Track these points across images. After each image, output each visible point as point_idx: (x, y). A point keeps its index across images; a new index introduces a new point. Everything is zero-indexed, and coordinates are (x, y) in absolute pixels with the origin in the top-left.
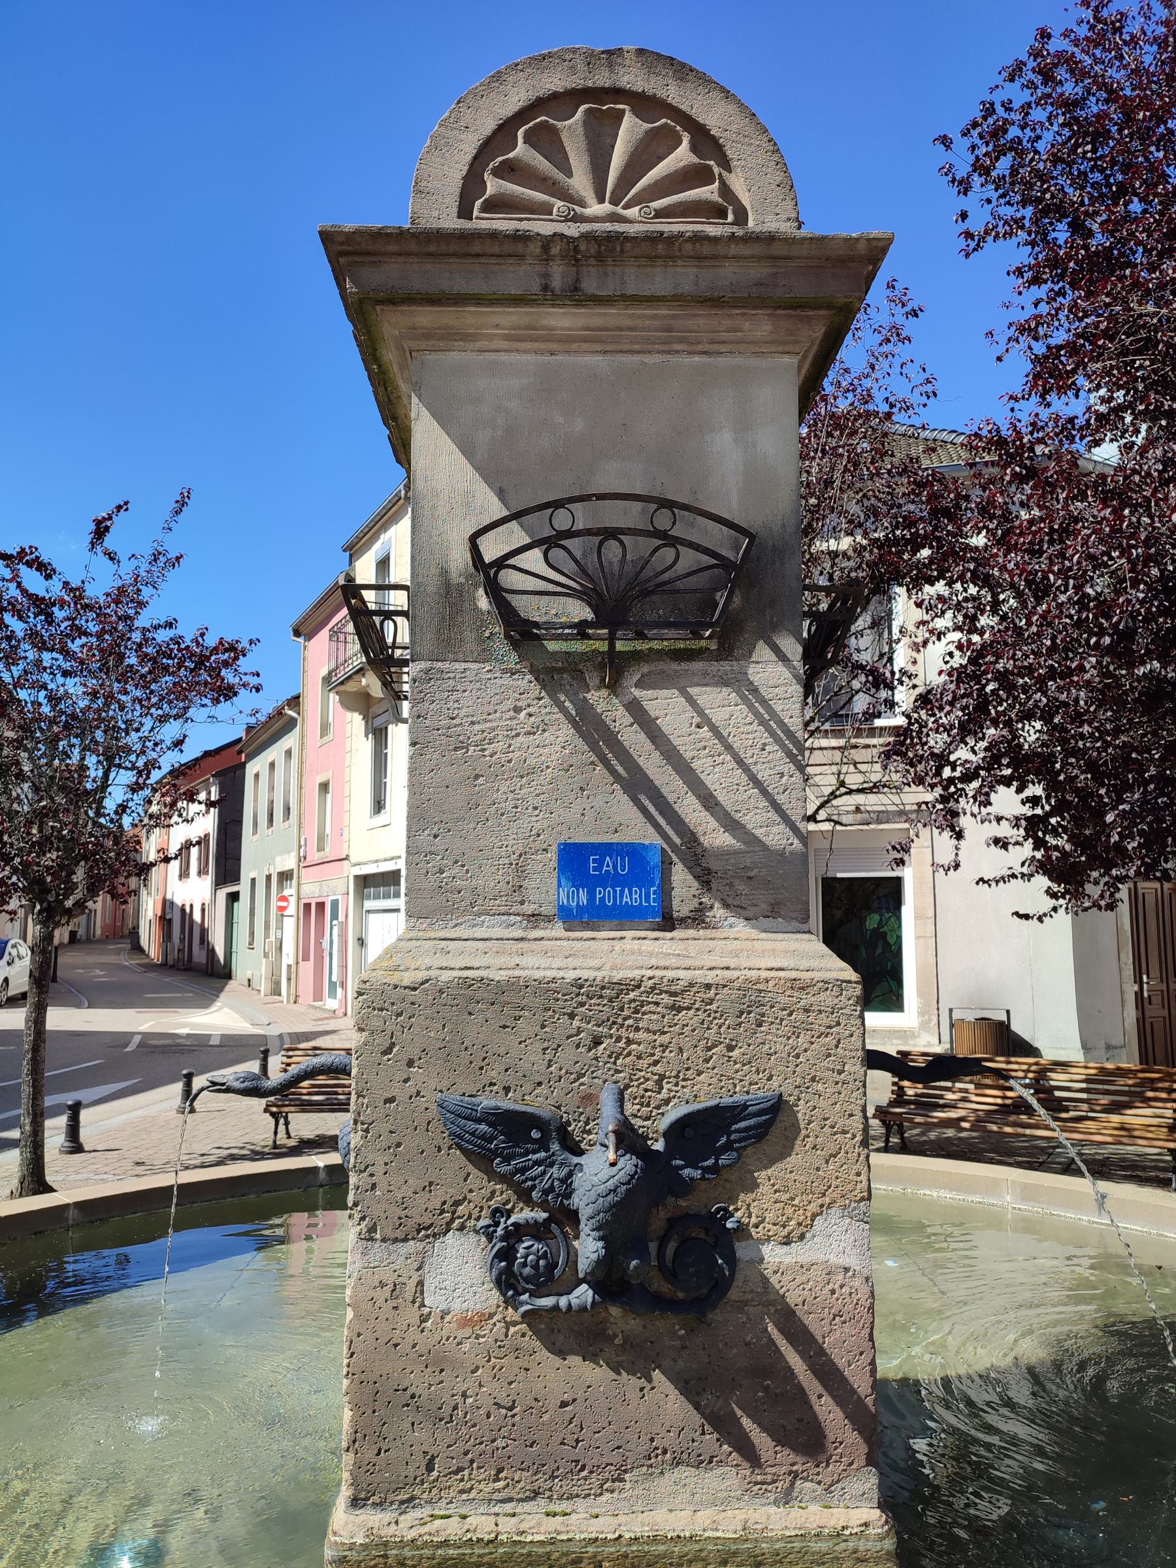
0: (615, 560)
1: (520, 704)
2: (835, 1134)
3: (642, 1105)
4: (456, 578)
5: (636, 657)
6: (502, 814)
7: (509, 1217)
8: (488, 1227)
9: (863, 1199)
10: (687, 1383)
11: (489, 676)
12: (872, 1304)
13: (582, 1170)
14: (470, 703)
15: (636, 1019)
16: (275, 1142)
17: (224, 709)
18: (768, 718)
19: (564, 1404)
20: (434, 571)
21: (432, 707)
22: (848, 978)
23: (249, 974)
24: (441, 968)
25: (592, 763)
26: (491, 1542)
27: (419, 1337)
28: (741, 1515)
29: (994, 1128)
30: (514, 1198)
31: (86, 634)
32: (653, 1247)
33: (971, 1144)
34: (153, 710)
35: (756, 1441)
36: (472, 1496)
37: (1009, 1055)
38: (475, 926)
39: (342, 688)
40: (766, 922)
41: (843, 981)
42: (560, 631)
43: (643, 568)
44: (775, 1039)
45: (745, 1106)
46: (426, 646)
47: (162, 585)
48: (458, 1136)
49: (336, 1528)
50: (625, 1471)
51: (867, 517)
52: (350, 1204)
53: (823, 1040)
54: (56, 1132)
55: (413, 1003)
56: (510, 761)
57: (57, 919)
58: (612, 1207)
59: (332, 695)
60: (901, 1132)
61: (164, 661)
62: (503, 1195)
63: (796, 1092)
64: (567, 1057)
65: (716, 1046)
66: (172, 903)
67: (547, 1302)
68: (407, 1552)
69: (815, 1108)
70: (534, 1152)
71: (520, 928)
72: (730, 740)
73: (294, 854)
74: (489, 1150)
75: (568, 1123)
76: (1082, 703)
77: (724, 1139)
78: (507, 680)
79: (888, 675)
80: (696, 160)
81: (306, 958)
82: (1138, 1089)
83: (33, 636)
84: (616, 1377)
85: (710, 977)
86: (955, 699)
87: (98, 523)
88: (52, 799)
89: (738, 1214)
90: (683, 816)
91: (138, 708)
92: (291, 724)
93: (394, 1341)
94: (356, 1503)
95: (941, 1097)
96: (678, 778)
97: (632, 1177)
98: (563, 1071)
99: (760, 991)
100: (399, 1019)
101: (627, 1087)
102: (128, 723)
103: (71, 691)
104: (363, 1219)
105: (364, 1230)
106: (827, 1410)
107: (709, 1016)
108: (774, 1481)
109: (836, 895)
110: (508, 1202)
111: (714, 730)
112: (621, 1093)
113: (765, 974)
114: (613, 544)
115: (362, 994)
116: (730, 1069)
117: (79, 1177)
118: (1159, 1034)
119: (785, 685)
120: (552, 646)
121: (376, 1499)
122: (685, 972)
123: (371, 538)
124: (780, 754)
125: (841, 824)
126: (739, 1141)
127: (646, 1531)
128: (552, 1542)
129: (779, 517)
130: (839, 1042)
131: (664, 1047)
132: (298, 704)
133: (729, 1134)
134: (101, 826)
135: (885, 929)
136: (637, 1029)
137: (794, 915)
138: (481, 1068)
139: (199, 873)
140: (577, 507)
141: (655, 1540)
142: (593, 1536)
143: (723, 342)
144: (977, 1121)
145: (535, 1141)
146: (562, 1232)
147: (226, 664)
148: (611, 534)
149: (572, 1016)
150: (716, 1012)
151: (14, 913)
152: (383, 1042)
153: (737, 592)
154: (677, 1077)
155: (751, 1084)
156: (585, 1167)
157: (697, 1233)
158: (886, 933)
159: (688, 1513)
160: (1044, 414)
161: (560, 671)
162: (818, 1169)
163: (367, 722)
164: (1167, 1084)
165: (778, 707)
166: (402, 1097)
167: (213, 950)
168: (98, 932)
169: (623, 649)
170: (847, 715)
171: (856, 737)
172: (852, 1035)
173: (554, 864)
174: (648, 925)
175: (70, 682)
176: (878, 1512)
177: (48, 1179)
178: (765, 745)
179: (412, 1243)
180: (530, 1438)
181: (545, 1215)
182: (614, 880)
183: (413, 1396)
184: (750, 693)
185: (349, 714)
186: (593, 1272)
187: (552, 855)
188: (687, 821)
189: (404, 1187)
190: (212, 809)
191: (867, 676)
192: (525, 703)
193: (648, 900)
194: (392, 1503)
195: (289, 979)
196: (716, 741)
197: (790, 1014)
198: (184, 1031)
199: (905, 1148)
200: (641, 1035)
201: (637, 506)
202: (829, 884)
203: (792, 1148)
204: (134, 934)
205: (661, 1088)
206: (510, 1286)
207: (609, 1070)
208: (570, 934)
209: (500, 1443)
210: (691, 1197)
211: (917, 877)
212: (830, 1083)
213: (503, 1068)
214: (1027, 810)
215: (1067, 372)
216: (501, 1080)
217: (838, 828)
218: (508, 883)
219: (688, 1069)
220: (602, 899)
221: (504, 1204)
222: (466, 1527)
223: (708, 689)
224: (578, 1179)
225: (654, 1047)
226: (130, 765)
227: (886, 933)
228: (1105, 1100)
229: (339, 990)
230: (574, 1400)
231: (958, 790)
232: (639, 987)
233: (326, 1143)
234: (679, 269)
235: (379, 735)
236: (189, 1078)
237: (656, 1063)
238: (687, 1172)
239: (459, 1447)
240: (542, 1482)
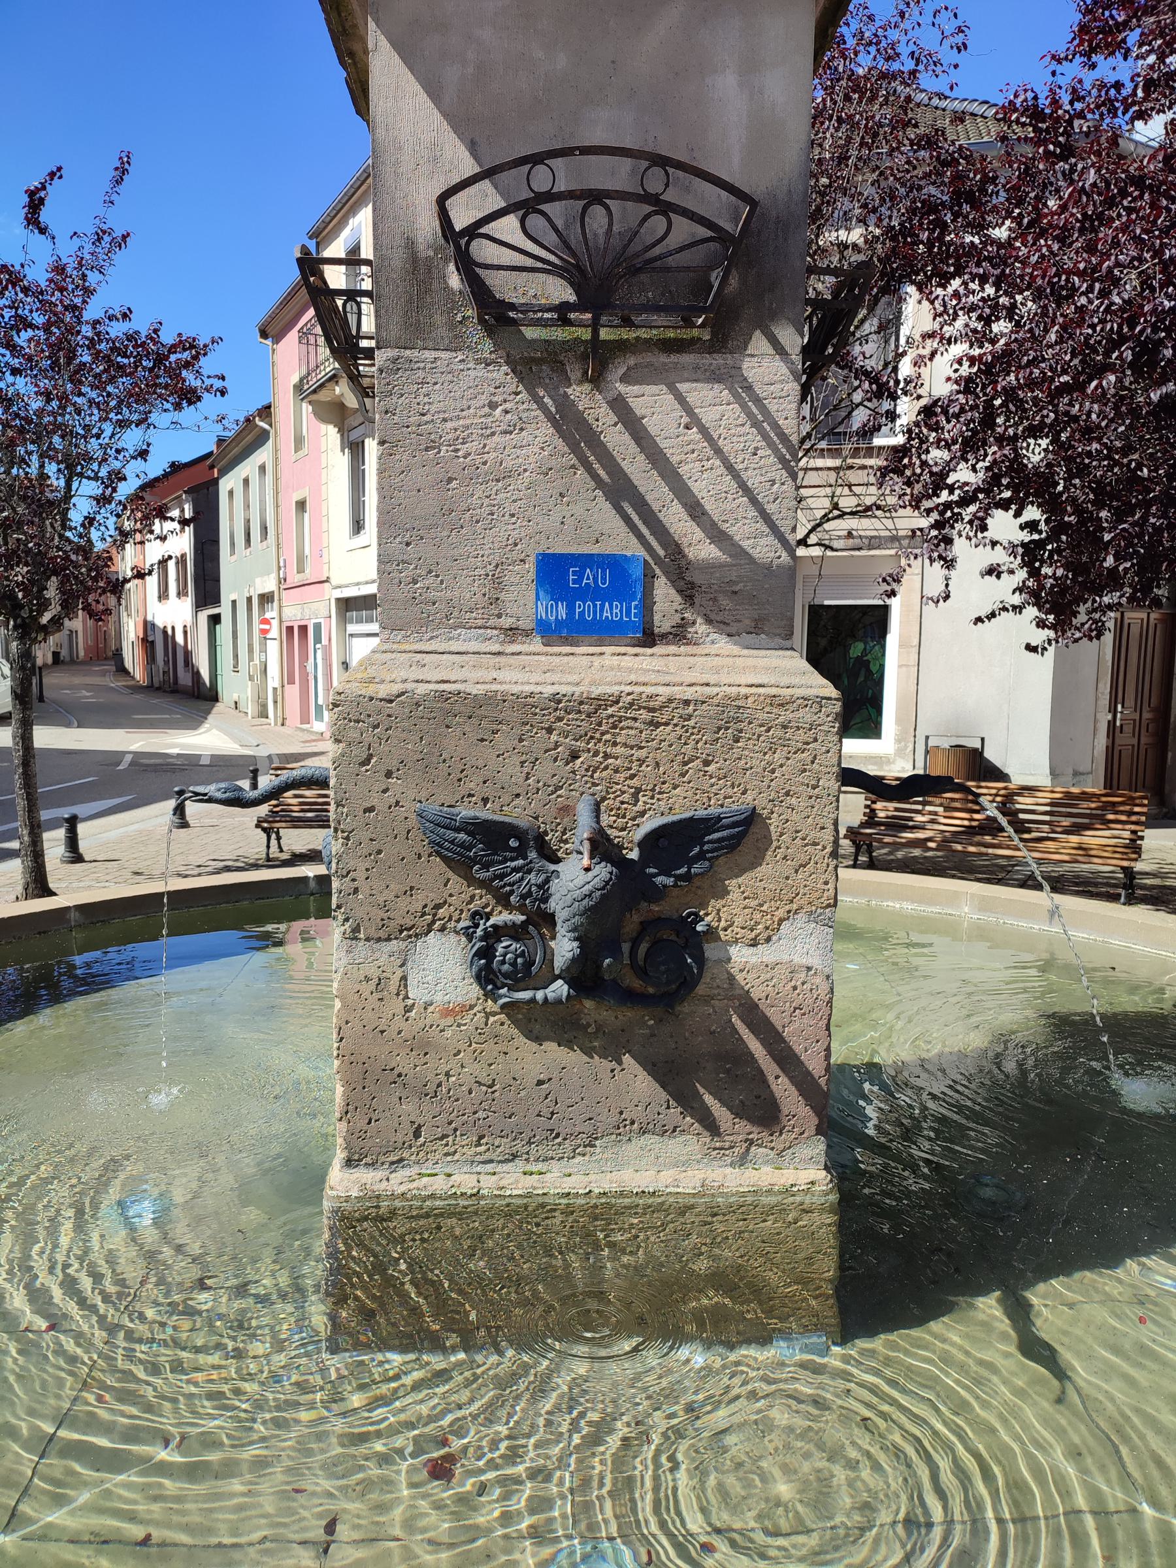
0: (601, 232)
1: (495, 399)
2: (806, 845)
3: (618, 817)
4: (424, 251)
5: (622, 347)
6: (478, 522)
7: (488, 919)
8: (468, 928)
9: (829, 906)
11: (461, 367)
12: (831, 999)
13: (558, 877)
14: (441, 398)
15: (613, 734)
16: (268, 854)
17: (188, 414)
19: (540, 1083)
20: (399, 241)
21: (400, 401)
22: (828, 695)
23: (235, 697)
24: (417, 681)
25: (573, 466)
26: (472, 1195)
27: (404, 1025)
28: (700, 1175)
29: (959, 847)
30: (493, 902)
31: (31, 326)
32: (626, 947)
33: (935, 863)
34: (112, 415)
37: (979, 780)
39: (314, 397)
43: (630, 241)
45: (719, 819)
46: (394, 331)
47: (109, 271)
48: (438, 844)
49: (332, 1183)
50: (596, 1139)
51: (883, 200)
52: (334, 906)
53: (800, 756)
54: (56, 843)
55: (389, 716)
56: (485, 463)
57: (34, 635)
59: (304, 405)
60: (870, 851)
61: (119, 359)
62: (483, 899)
63: (770, 806)
65: (692, 761)
66: (153, 625)
67: (525, 995)
68: (397, 1203)
69: (787, 821)
70: (512, 860)
72: (721, 442)
73: (273, 576)
74: (469, 858)
76: (1094, 416)
77: (697, 849)
78: (481, 372)
79: (892, 383)
81: (291, 681)
82: (1099, 812)
84: (589, 1060)
85: (690, 693)
86: (962, 410)
87: (31, 194)
88: (14, 509)
89: (708, 919)
90: (668, 525)
91: (96, 411)
92: (263, 437)
93: (381, 1028)
94: (349, 1163)
95: (911, 819)
96: (663, 484)
97: (607, 883)
98: (541, 784)
99: (739, 707)
100: (376, 731)
101: (604, 799)
102: (87, 428)
103: (22, 391)
104: (347, 920)
105: (349, 931)
106: (782, 1088)
107: (687, 731)
108: (731, 1147)
109: (822, 623)
110: (487, 905)
111: (704, 431)
112: (597, 805)
113: (744, 691)
114: (597, 211)
115: (338, 706)
116: (706, 783)
117: (82, 884)
118: (1126, 762)
119: (782, 382)
120: (530, 333)
121: (368, 1160)
123: (339, 222)
124: (773, 459)
125: (832, 549)
126: (712, 851)
127: (615, 1187)
128: (529, 1195)
129: (785, 182)
130: (815, 757)
131: (641, 761)
132: (269, 415)
133: (702, 846)
134: (68, 540)
135: (869, 657)
136: (615, 744)
138: (460, 780)
139: (179, 595)
140: (557, 163)
141: (622, 1194)
142: (566, 1191)
145: (513, 850)
146: (539, 933)
147: (187, 365)
148: (596, 197)
149: (550, 730)
152: (360, 753)
153: (734, 272)
154: (653, 790)
155: (725, 798)
157: (668, 935)
158: (868, 662)
160: (1089, 78)
161: (539, 362)
162: (787, 878)
163: (342, 436)
164: (1127, 808)
165: (772, 407)
166: (381, 806)
167: (198, 672)
168: (82, 653)
170: (845, 433)
171: (853, 457)
172: (828, 752)
173: (532, 575)
174: (629, 641)
175: (20, 381)
176: (824, 1173)
177: (51, 885)
178: (757, 449)
179: (395, 942)
180: (509, 1111)
181: (523, 918)
182: (595, 594)
183: (400, 1075)
184: (743, 392)
187: (531, 566)
188: (672, 531)
189: (386, 891)
190: (187, 528)
191: (871, 384)
193: (628, 614)
194: (383, 1164)
195: (275, 702)
196: (706, 444)
197: (768, 731)
198: (175, 751)
199: (872, 865)
200: (619, 750)
201: (626, 164)
202: (816, 612)
204: (118, 656)
206: (489, 982)
207: (586, 782)
208: (549, 649)
209: (481, 1114)
210: (663, 903)
211: (905, 606)
213: (482, 780)
214: (1025, 537)
215: (1117, 24)
216: (480, 791)
217: (829, 553)
218: (484, 595)
219: (664, 783)
220: (582, 614)
221: (483, 908)
222: (451, 1183)
223: (699, 385)
224: (554, 885)
225: (631, 762)
226: (92, 475)
227: (868, 662)
228: (1066, 822)
230: (550, 1079)
232: (617, 702)
233: (313, 856)
235: (356, 449)
237: (632, 777)
238: (660, 880)
240: (519, 1146)
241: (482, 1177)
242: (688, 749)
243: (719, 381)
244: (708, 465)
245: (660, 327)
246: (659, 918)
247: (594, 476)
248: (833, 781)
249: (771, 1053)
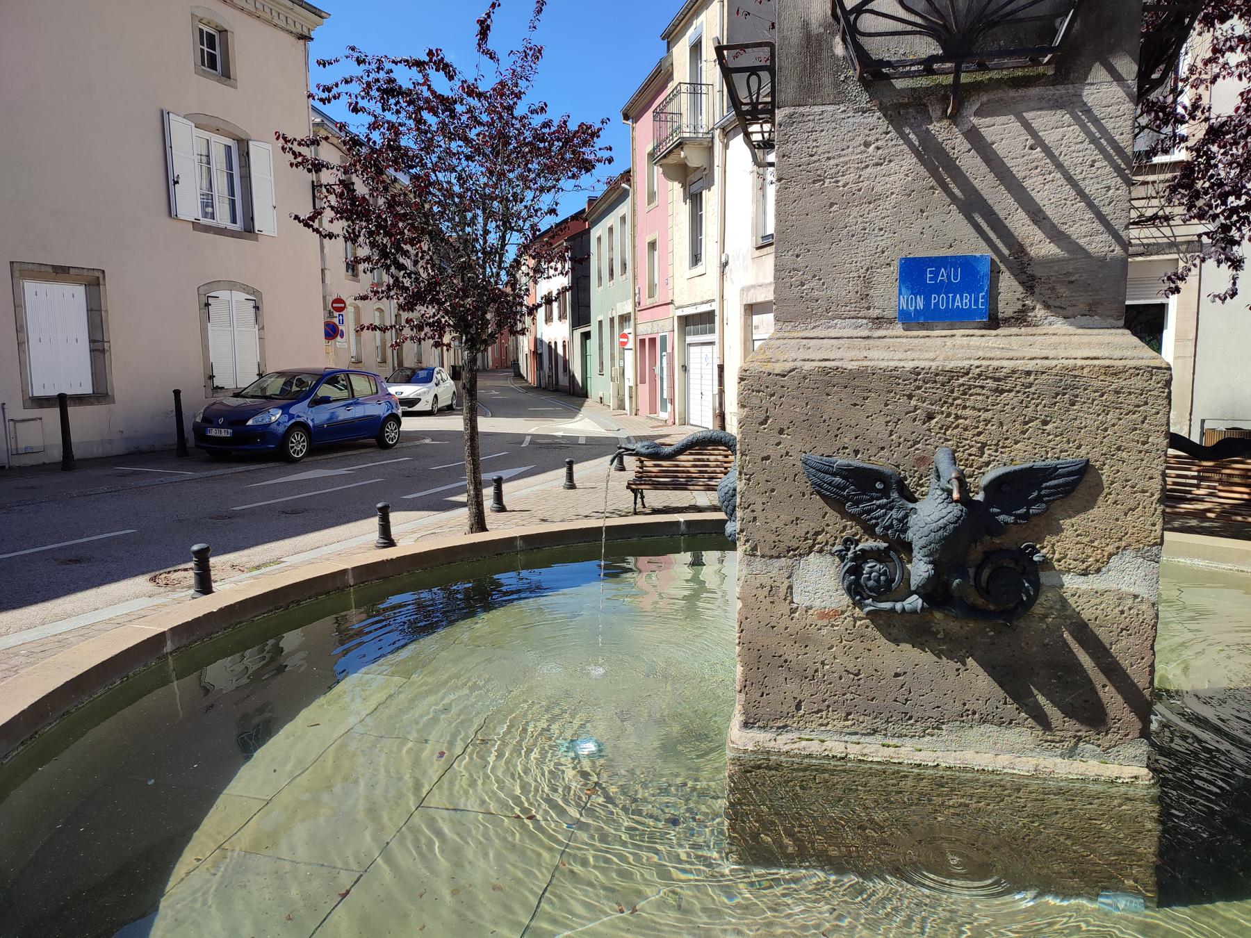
1: (870, 139)
4: (816, 29)
5: (977, 87)
6: (853, 236)
7: (857, 545)
9: (1155, 544)
10: (994, 668)
11: (843, 116)
12: (1156, 623)
14: (826, 142)
17: (585, 179)
18: (1099, 137)
19: (897, 675)
23: (601, 394)
25: (932, 188)
26: (843, 758)
27: (789, 623)
28: (1033, 761)
31: (480, 124)
35: (1049, 713)
36: (828, 728)
38: (829, 328)
39: (664, 161)
40: (1084, 320)
41: (1153, 368)
42: (908, 68)
44: (1086, 416)
45: (1056, 469)
48: (818, 485)
49: (733, 739)
50: (943, 723)
55: (783, 387)
56: (859, 190)
58: (940, 540)
62: (853, 529)
63: (1102, 459)
64: (905, 428)
66: (542, 341)
67: (887, 605)
68: (783, 758)
69: (1118, 471)
70: (878, 499)
71: (866, 329)
72: (1061, 159)
73: (631, 301)
75: (905, 479)
77: (1035, 494)
78: (859, 118)
81: (643, 382)
83: (443, 126)
84: (937, 659)
85: (1031, 366)
87: (481, 22)
88: (469, 256)
89: (1044, 551)
90: (1012, 230)
92: (624, 195)
93: (772, 624)
94: (746, 725)
97: (959, 518)
98: (902, 439)
99: (1076, 377)
104: (747, 541)
106: (1110, 696)
108: (1061, 741)
110: (856, 534)
111: (1047, 151)
113: (1080, 363)
116: (1044, 439)
119: (1118, 104)
120: (899, 84)
121: (760, 724)
122: (1008, 362)
123: (685, 24)
124: (1109, 169)
127: (958, 764)
130: (1145, 418)
131: (987, 422)
133: (1040, 490)
136: (965, 407)
137: (1111, 313)
138: (836, 436)
139: (560, 318)
141: (965, 770)
142: (918, 762)
144: (1222, 512)
149: (910, 397)
150: (1034, 394)
151: (449, 345)
153: (1079, 20)
155: (1061, 452)
156: (919, 511)
159: (991, 755)
161: (906, 106)
162: (1117, 520)
163: (685, 189)
165: (1109, 125)
168: (490, 364)
169: (968, 80)
172: (1158, 413)
173: (896, 275)
174: (976, 325)
176: (1146, 770)
178: (1094, 161)
179: (783, 559)
180: (872, 695)
182: (948, 288)
185: (670, 183)
186: (923, 586)
187: (895, 268)
188: (1016, 234)
192: (874, 138)
193: (976, 303)
194: (771, 728)
195: (631, 397)
196: (1048, 161)
197: (1102, 395)
198: (560, 434)
200: (968, 412)
203: (1095, 503)
204: (516, 365)
205: (983, 453)
206: (858, 593)
207: (940, 438)
208: (909, 333)
211: (1182, 307)
216: (853, 444)
219: (1007, 439)
220: (937, 304)
222: (824, 748)
229: (669, 405)
230: (905, 673)
231: (1240, 218)
232: (967, 374)
236: (570, 465)
237: (979, 434)
239: (819, 697)
240: (879, 724)
241: (849, 745)
242: (1029, 412)
244: (1050, 177)
248: (1162, 438)
249: (1098, 665)
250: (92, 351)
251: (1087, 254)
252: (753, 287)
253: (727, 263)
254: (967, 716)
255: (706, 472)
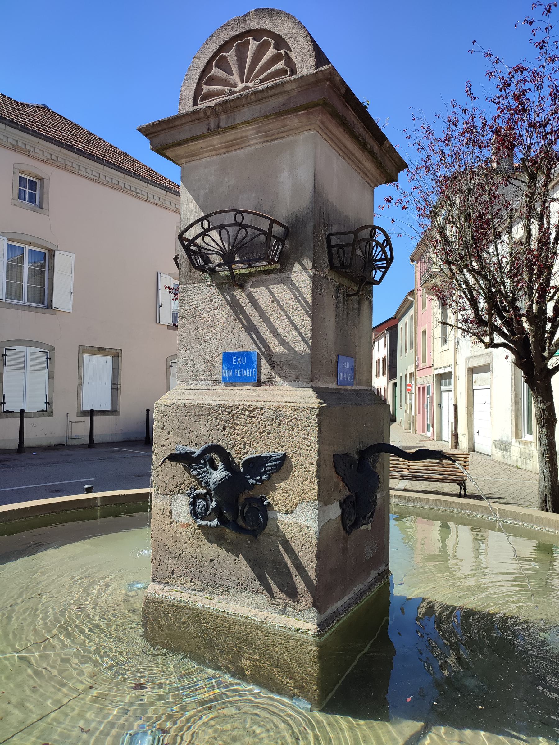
1: (212, 298)
8: (188, 493)
10: (250, 561)
15: (237, 421)
19: (211, 560)
25: (235, 320)
27: (170, 529)
28: (266, 614)
30: (197, 484)
39: (425, 285)
44: (285, 430)
45: (271, 457)
53: (303, 432)
63: (292, 453)
73: (414, 365)
77: (263, 469)
78: (208, 289)
80: (276, 51)
81: (419, 413)
85: (264, 405)
89: (269, 500)
97: (222, 479)
99: (280, 411)
106: (298, 581)
108: (279, 605)
119: (305, 281)
124: (303, 311)
126: (269, 470)
127: (233, 611)
130: (309, 433)
131: (246, 432)
132: (413, 294)
133: (266, 467)
136: (238, 424)
137: (305, 380)
143: (282, 132)
149: (217, 418)
154: (250, 443)
157: (255, 505)
162: (299, 485)
165: (302, 290)
176: (316, 626)
178: (297, 307)
182: (242, 367)
184: (292, 286)
197: (291, 421)
200: (239, 427)
209: (193, 570)
212: (305, 450)
220: (237, 374)
225: (243, 432)
232: (238, 408)
234: (254, 107)
237: (243, 438)
240: (204, 586)
241: (192, 596)
242: (262, 428)
243: (283, 283)
244: (279, 315)
245: (262, 265)
246: (252, 498)
247: (242, 323)
249: (293, 563)
250: (113, 389)
251: (295, 352)
252: (471, 357)
253: (458, 343)
254: (242, 587)
255: (397, 468)
